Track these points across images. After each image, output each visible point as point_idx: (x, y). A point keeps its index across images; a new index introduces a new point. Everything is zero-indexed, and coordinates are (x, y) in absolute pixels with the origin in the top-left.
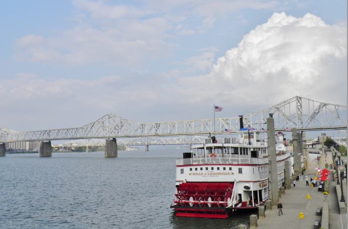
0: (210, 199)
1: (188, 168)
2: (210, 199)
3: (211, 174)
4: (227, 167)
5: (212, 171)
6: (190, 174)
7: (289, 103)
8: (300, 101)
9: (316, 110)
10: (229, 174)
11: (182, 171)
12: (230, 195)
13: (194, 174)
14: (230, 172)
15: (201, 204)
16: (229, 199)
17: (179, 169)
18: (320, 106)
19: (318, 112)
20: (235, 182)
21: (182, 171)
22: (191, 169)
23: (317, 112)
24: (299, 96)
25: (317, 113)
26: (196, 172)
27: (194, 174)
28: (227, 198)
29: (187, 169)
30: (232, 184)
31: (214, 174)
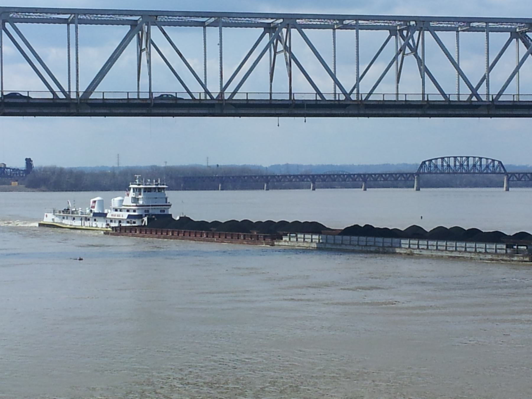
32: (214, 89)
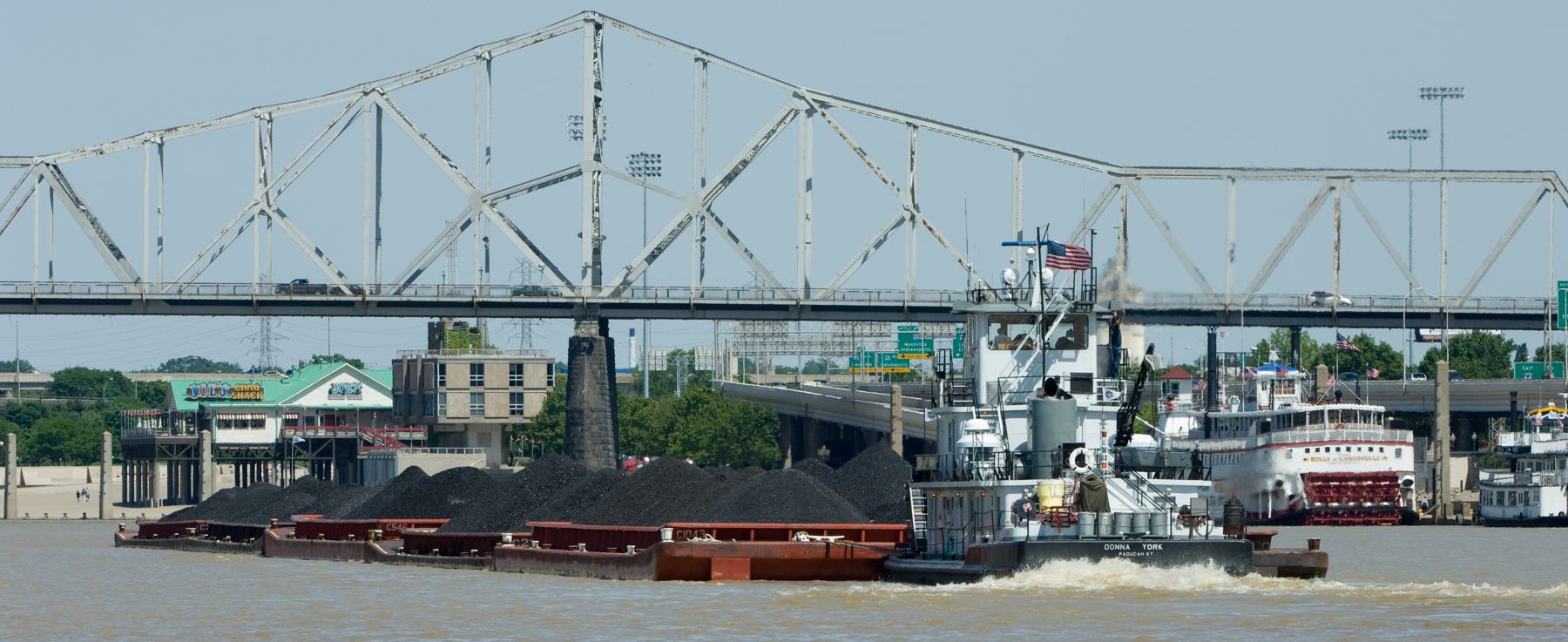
10: (1378, 459)
13: (1313, 459)
14: (1382, 455)
22: (1307, 451)
31: (1351, 459)
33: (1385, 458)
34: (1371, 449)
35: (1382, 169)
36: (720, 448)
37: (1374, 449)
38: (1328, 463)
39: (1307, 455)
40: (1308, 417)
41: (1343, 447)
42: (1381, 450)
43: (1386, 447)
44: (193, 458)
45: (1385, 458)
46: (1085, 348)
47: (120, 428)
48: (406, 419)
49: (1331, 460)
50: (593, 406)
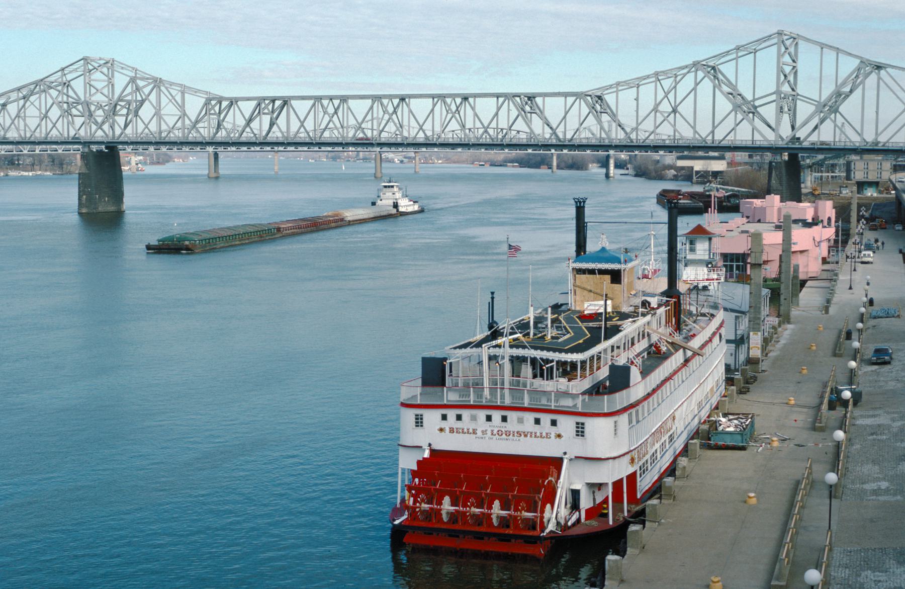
0: (447, 500)
1: (437, 414)
2: (447, 500)
3: (500, 433)
4: (546, 419)
5: (504, 424)
6: (441, 430)
7: (755, 51)
8: (792, 50)
9: (844, 83)
10: (548, 436)
11: (419, 421)
12: (550, 497)
13: (452, 430)
14: (553, 431)
15: (474, 516)
16: (548, 506)
17: (409, 415)
18: (859, 69)
19: (851, 91)
20: (565, 462)
21: (419, 421)
22: (444, 417)
23: (847, 89)
24: (788, 30)
25: (847, 96)
26: (459, 424)
27: (452, 430)
28: (544, 507)
29: (432, 417)
30: (557, 463)
31: (508, 433)
32: (870, 137)
33: (559, 436)
34: (537, 421)
35: (499, 112)
36: (612, 363)
37: (464, 418)
38: (473, 436)
39: (444, 424)
40: (673, 351)
41: (497, 415)
42: (504, 419)
43: (560, 419)
44: (735, 264)
45: (559, 436)
46: (657, 203)
47: (280, 228)
48: (793, 157)
49: (479, 433)
50: (775, 188)
